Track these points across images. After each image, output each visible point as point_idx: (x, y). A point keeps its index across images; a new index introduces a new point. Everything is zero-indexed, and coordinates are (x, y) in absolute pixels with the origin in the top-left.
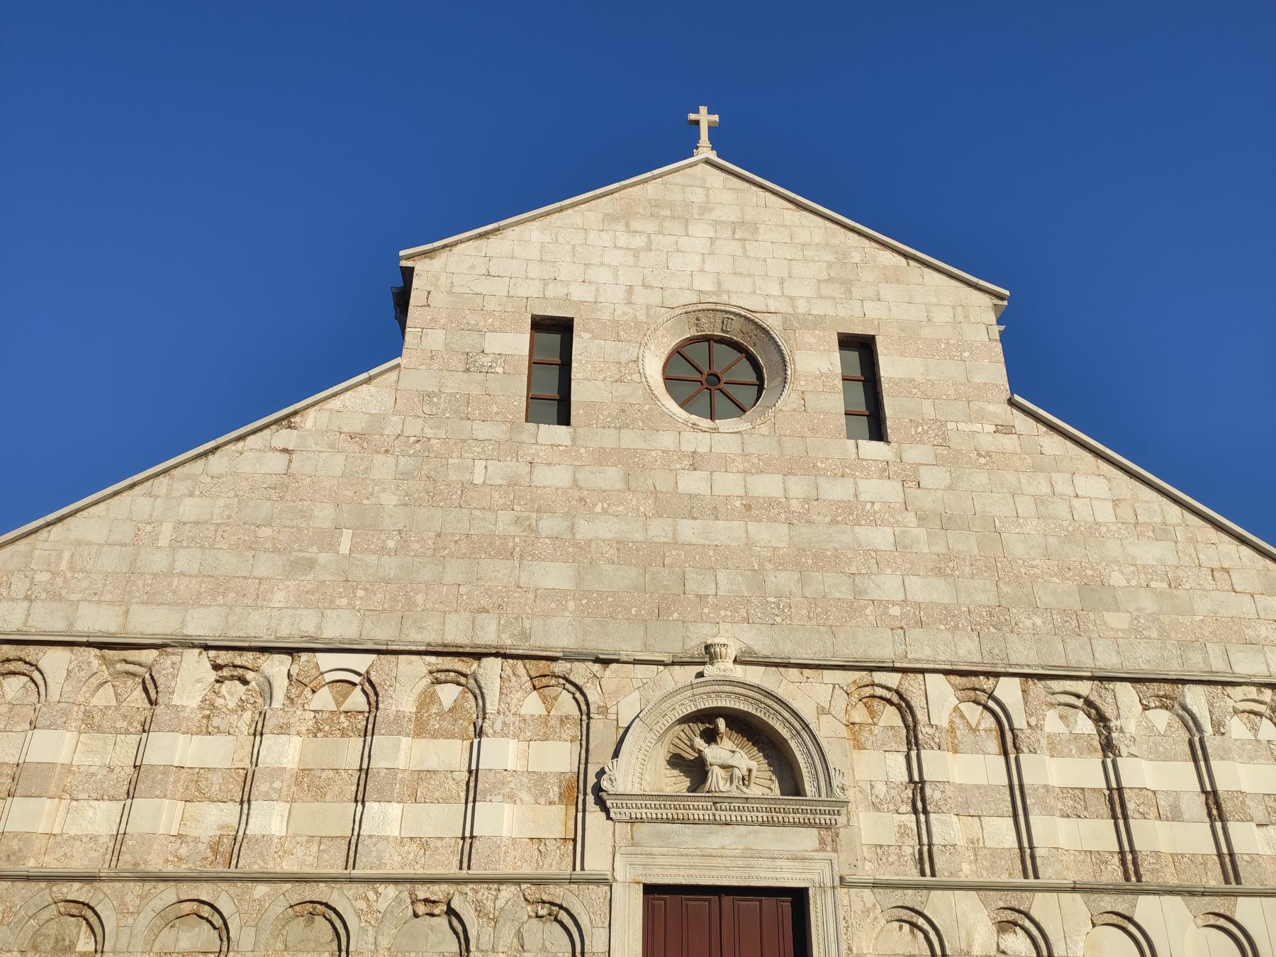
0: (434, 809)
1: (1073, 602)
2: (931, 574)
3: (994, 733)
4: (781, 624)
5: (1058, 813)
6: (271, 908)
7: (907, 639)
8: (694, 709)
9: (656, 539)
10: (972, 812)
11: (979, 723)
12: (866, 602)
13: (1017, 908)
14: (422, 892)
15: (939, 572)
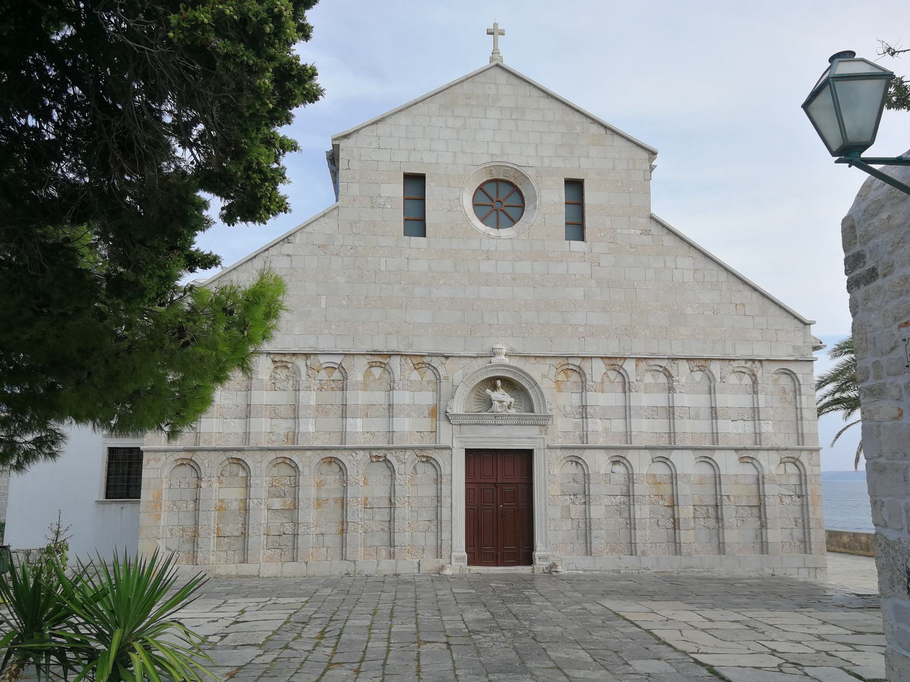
10: (607, 418)
11: (615, 379)
14: (374, 453)
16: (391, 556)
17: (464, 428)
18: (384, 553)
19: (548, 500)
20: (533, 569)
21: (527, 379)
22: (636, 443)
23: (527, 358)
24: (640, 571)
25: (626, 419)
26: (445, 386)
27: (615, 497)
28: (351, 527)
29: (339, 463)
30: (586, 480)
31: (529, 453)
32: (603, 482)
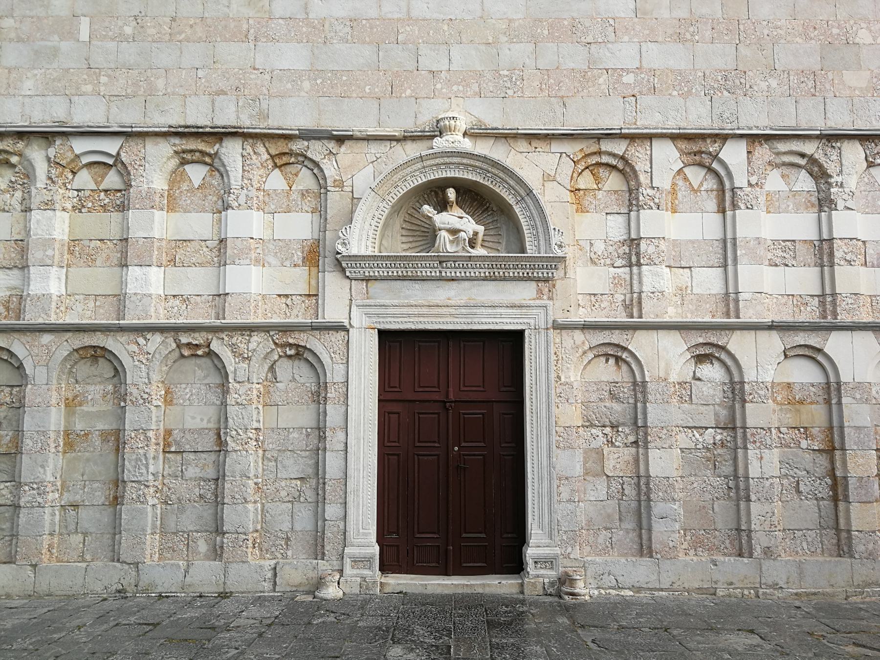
0: (194, 272)
1: (813, 62)
2: (670, 39)
3: (715, 193)
4: (513, 97)
5: (767, 263)
6: (57, 352)
7: (638, 106)
8: (424, 180)
9: (390, 16)
10: (684, 264)
11: (701, 184)
12: (600, 71)
13: (716, 343)
14: (184, 339)
15: (679, 38)
16: (217, 553)
17: (375, 287)
18: (203, 547)
19: (555, 438)
20: (522, 585)
21: (512, 182)
22: (748, 315)
23: (511, 141)
24: (761, 591)
25: (725, 266)
26: (336, 201)
27: (701, 431)
28: (131, 492)
29: (112, 359)
30: (639, 395)
31: (515, 339)
32: (675, 400)
